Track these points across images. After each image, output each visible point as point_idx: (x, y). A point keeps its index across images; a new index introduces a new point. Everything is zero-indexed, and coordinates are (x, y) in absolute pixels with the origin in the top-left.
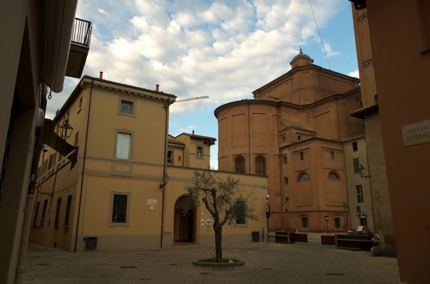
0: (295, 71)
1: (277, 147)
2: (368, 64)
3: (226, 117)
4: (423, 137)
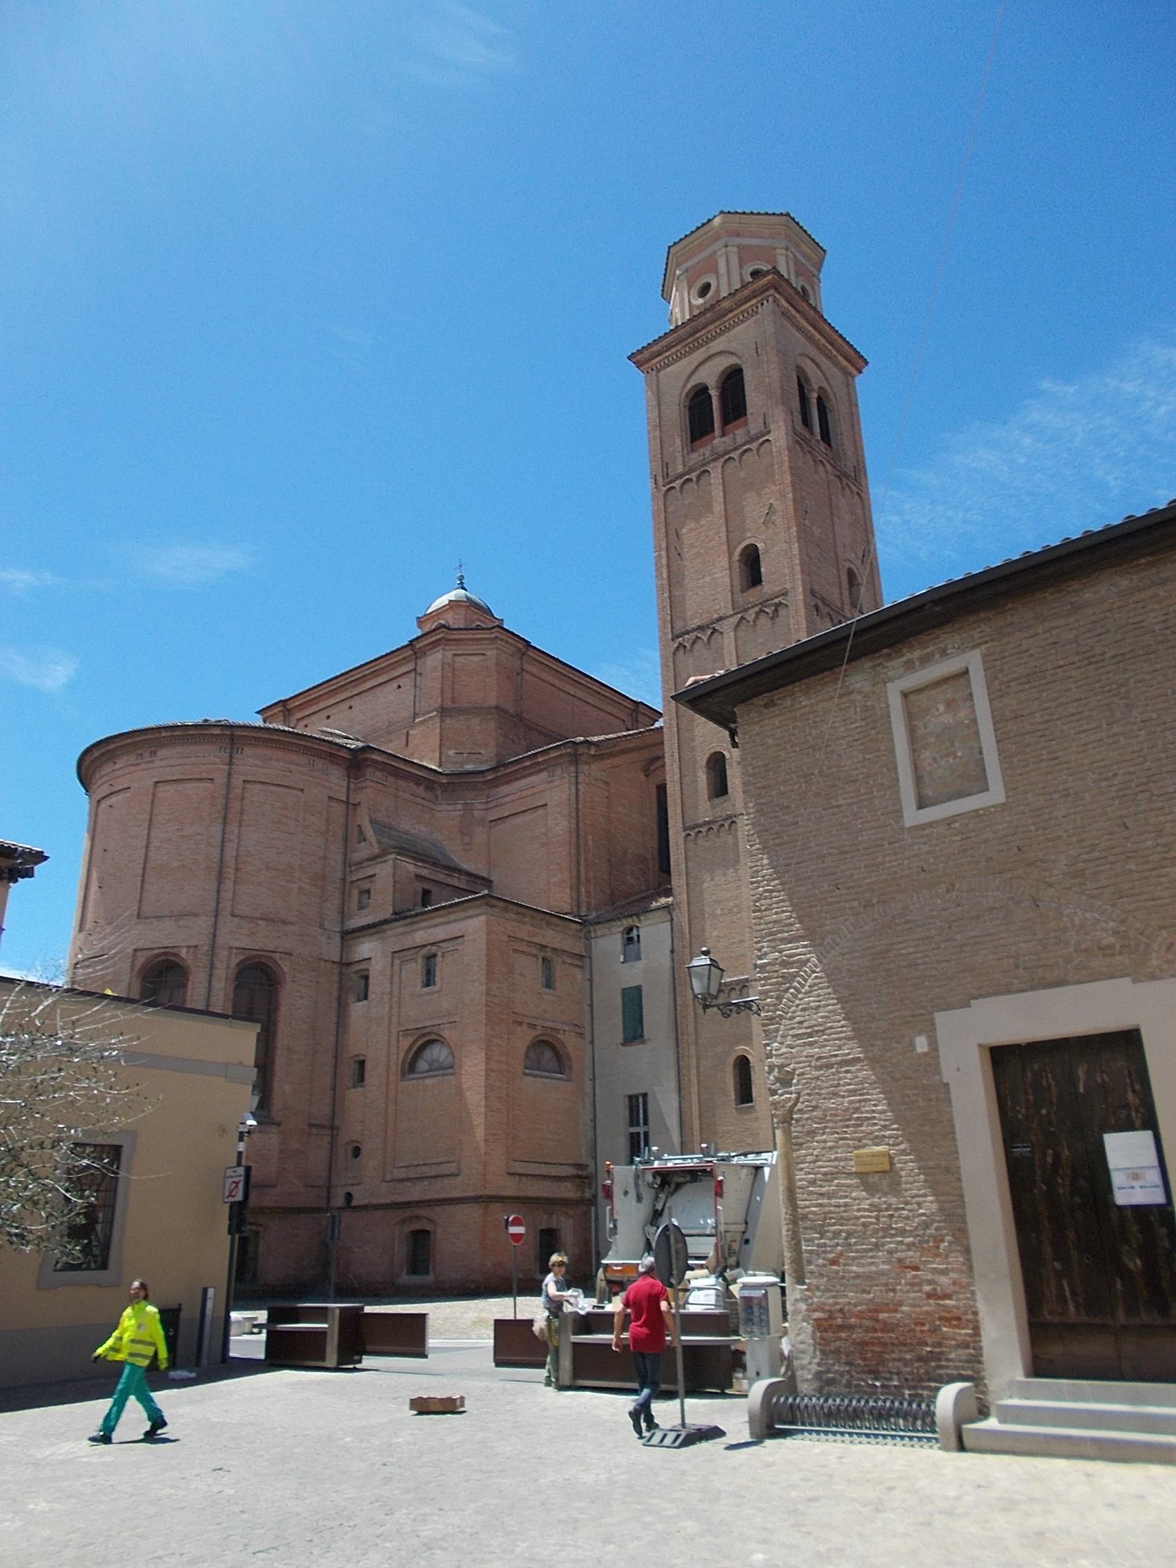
1: (333, 925)
2: (694, 643)
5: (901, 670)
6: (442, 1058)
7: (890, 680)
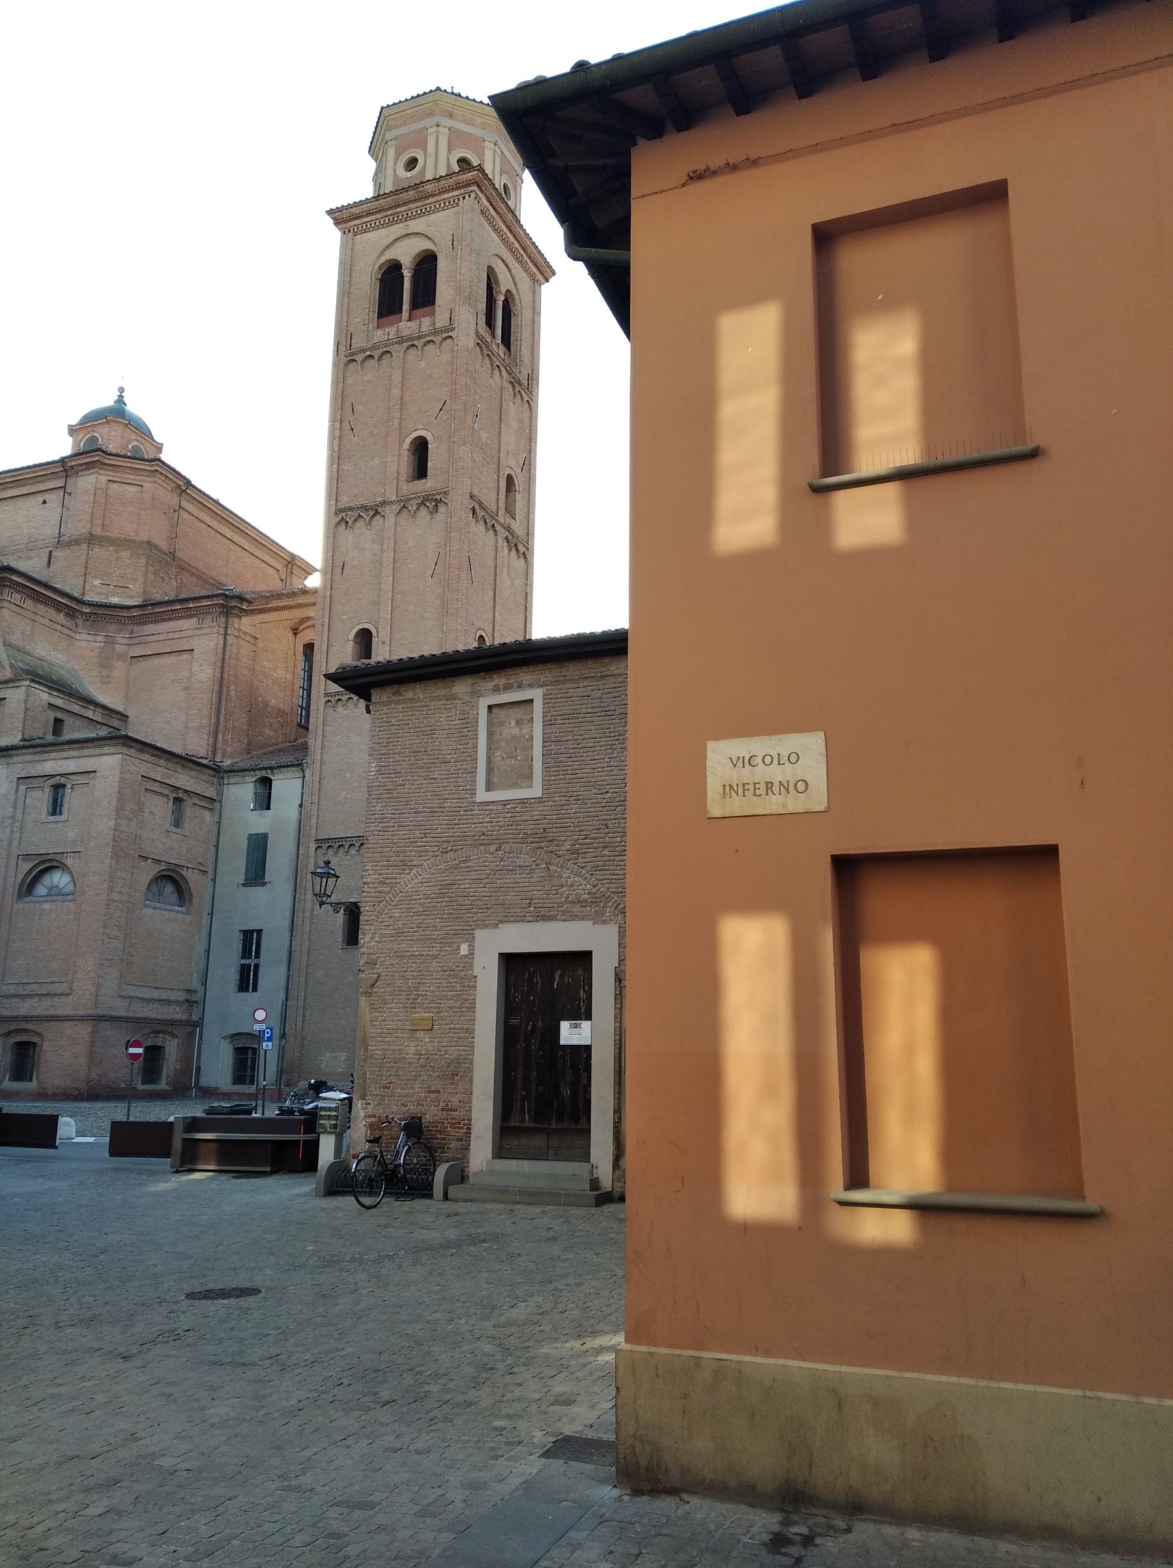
2: (355, 520)
4: (780, 794)
6: (61, 885)
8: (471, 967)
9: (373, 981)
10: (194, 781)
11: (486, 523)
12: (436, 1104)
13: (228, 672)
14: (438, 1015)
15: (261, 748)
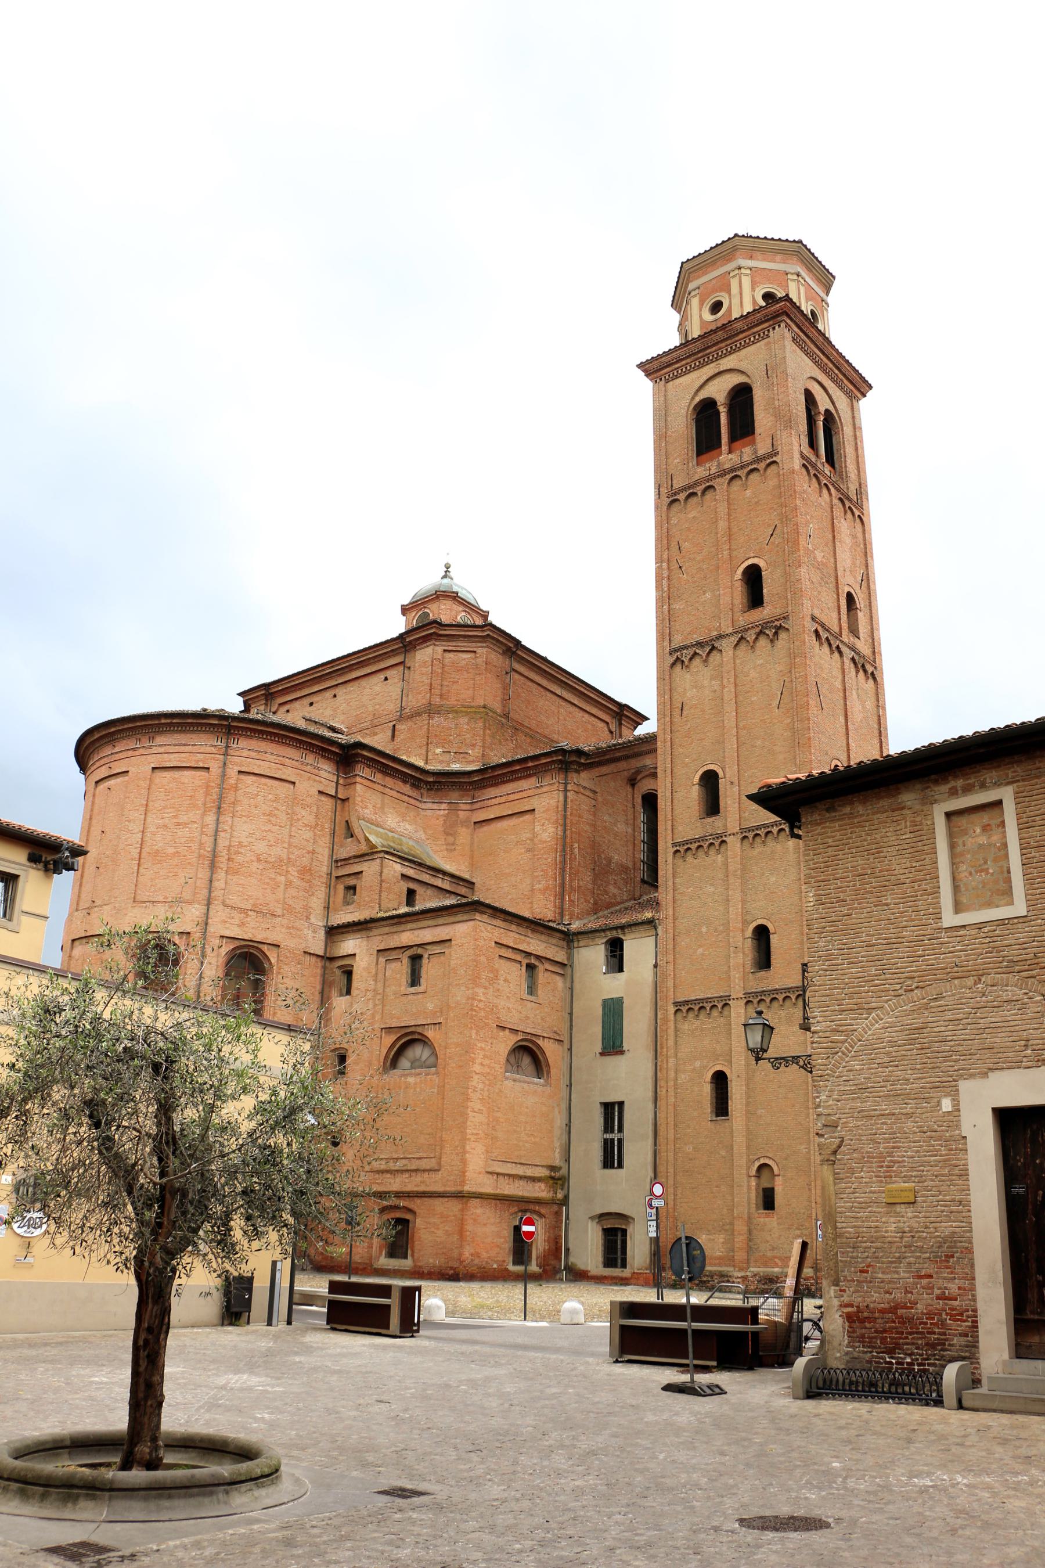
0: (423, 637)
1: (318, 921)
2: (691, 659)
3: (128, 772)
5: (947, 795)
7: (936, 801)
8: (958, 1126)
9: (835, 1146)
10: (545, 945)
11: (830, 645)
12: (929, 1291)
13: (571, 829)
14: (921, 1184)
15: (607, 908)
